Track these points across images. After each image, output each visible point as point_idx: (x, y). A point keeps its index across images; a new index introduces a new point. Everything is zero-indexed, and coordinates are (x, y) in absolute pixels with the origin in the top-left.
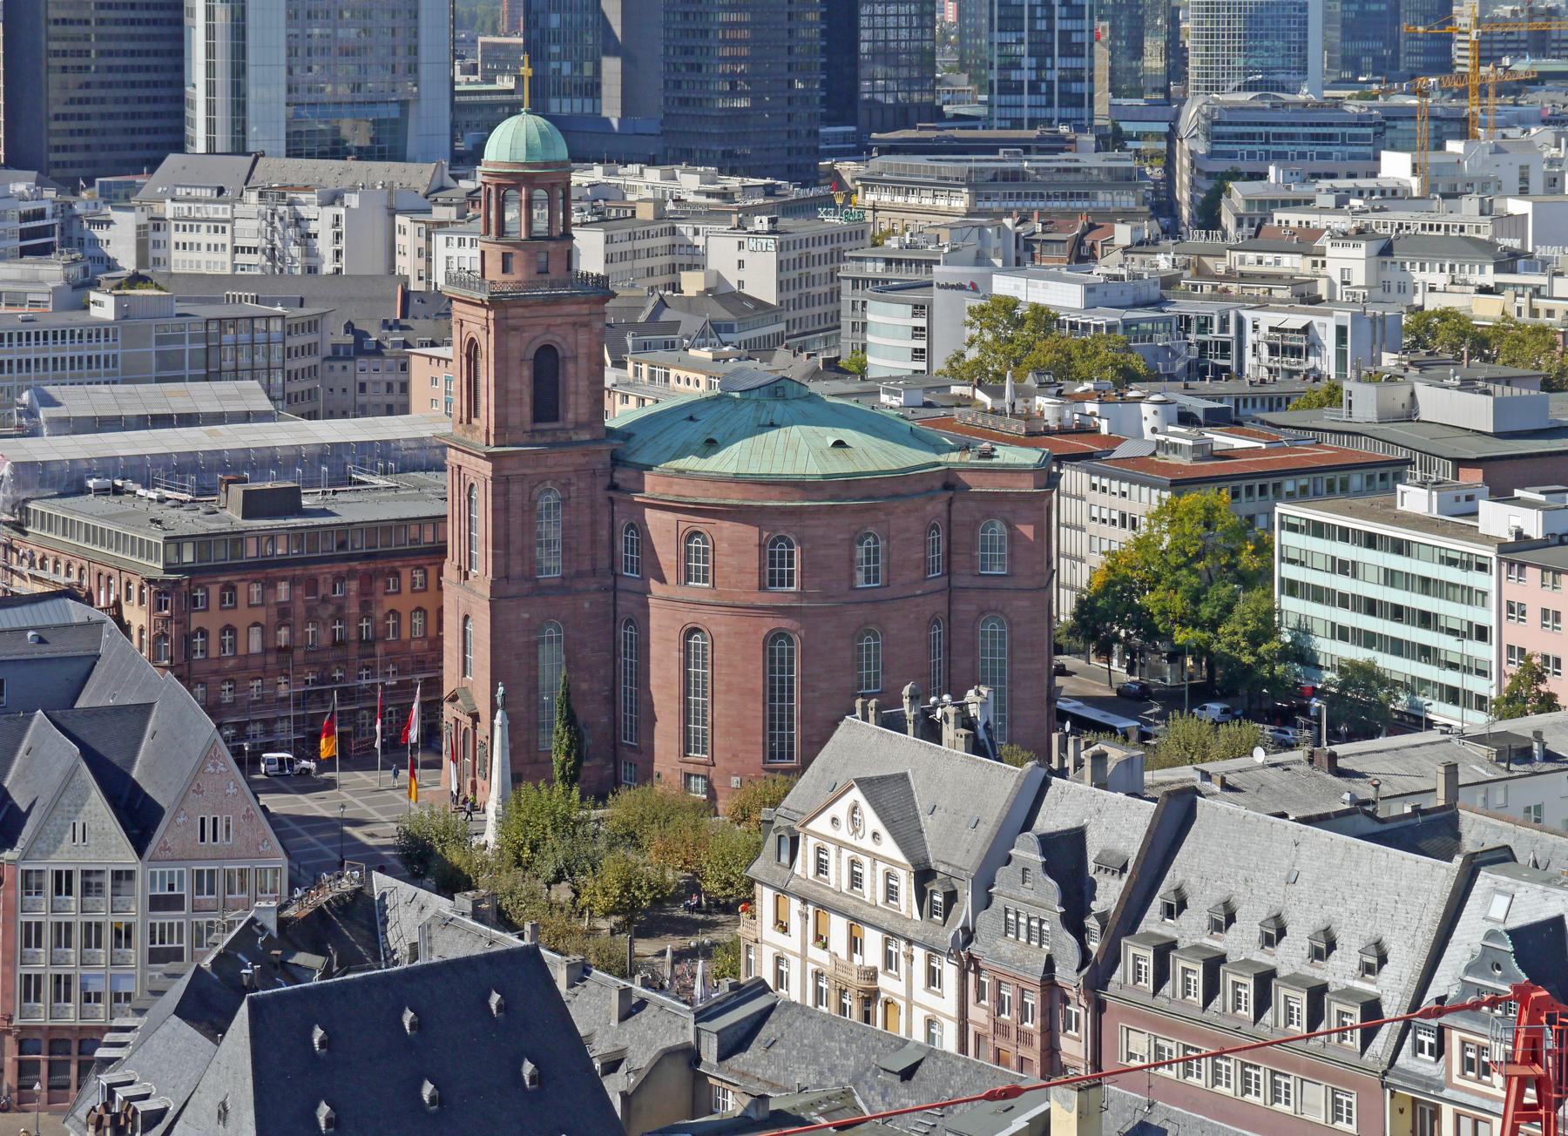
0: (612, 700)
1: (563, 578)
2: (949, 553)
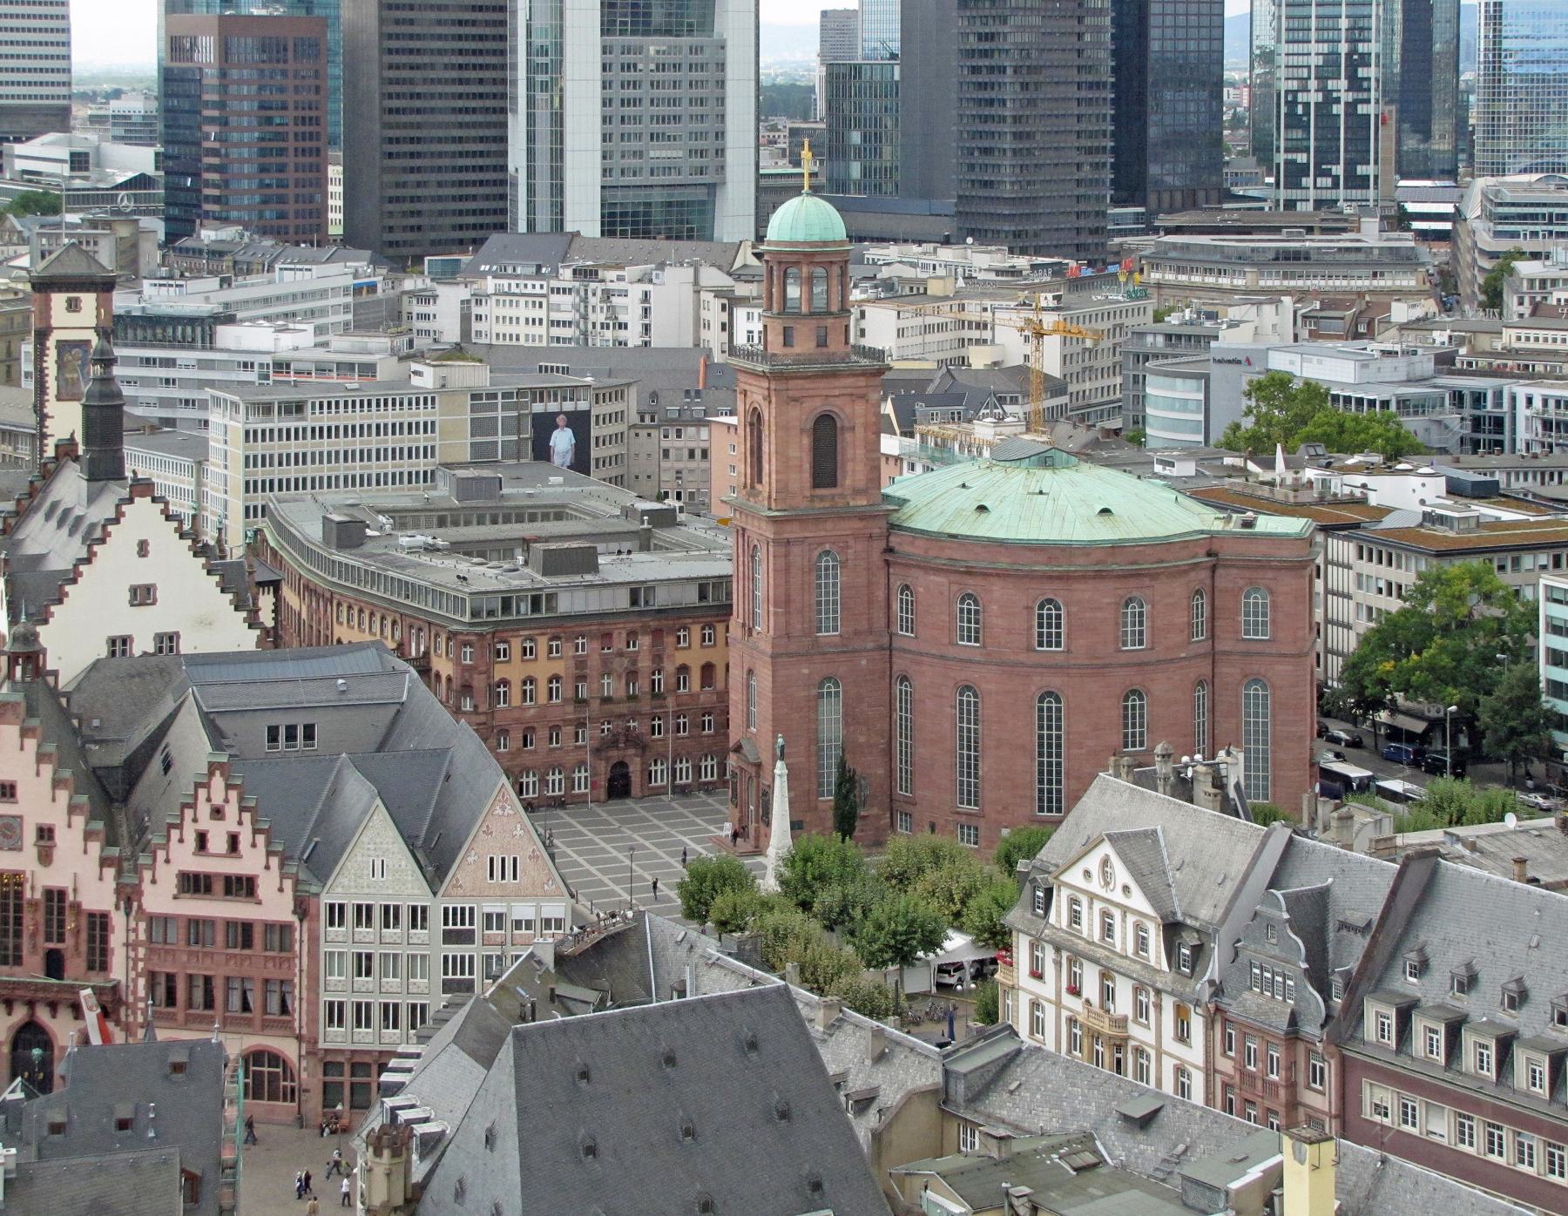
2: (1213, 618)
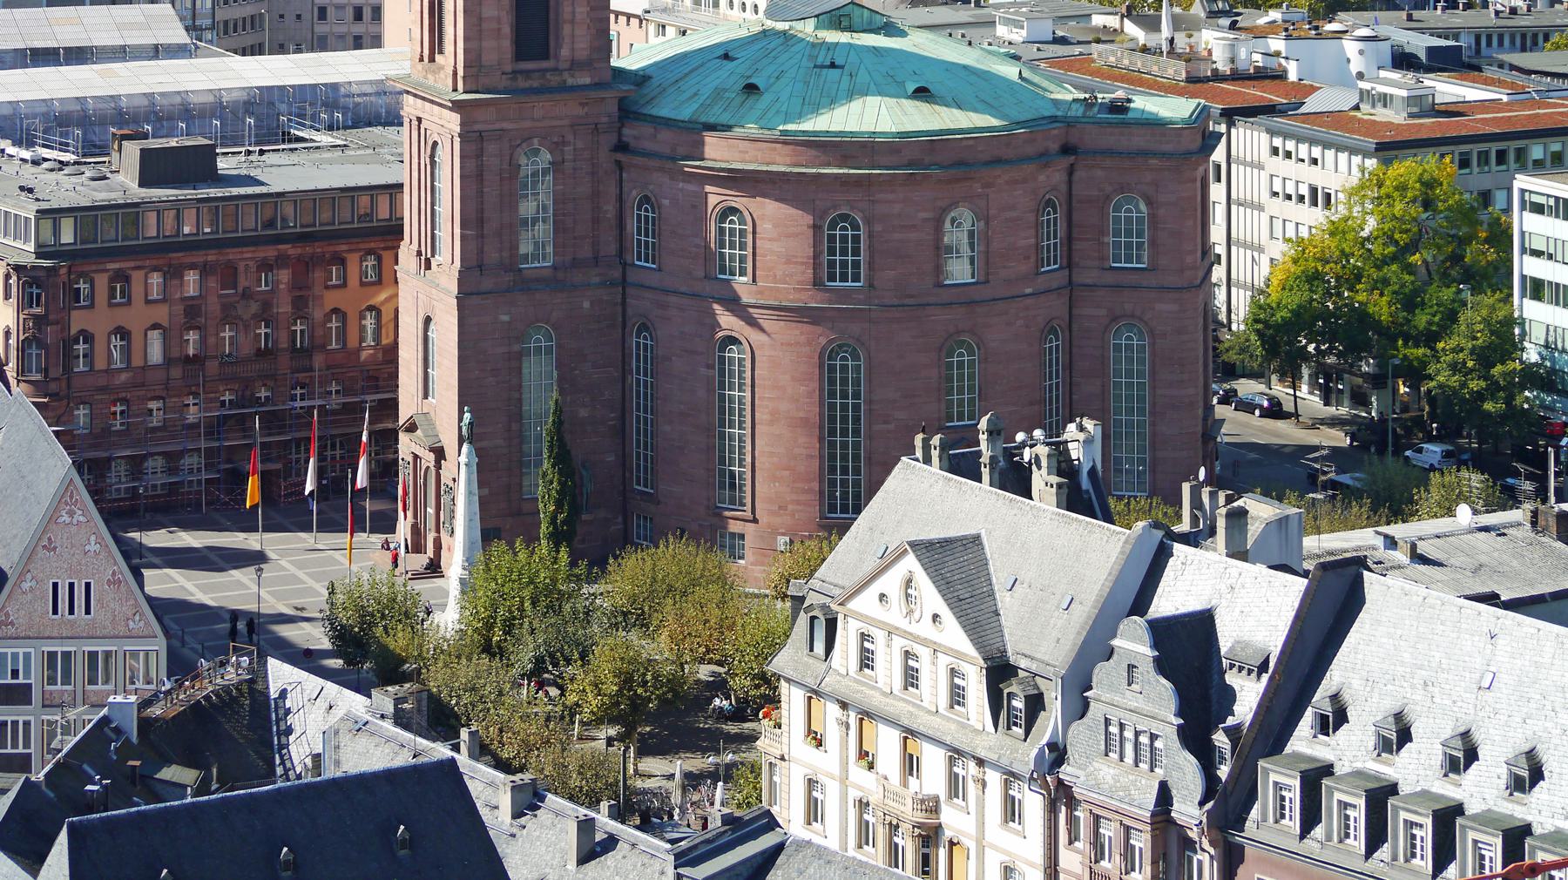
0: (621, 431)
1: (554, 267)
2: (1070, 239)
